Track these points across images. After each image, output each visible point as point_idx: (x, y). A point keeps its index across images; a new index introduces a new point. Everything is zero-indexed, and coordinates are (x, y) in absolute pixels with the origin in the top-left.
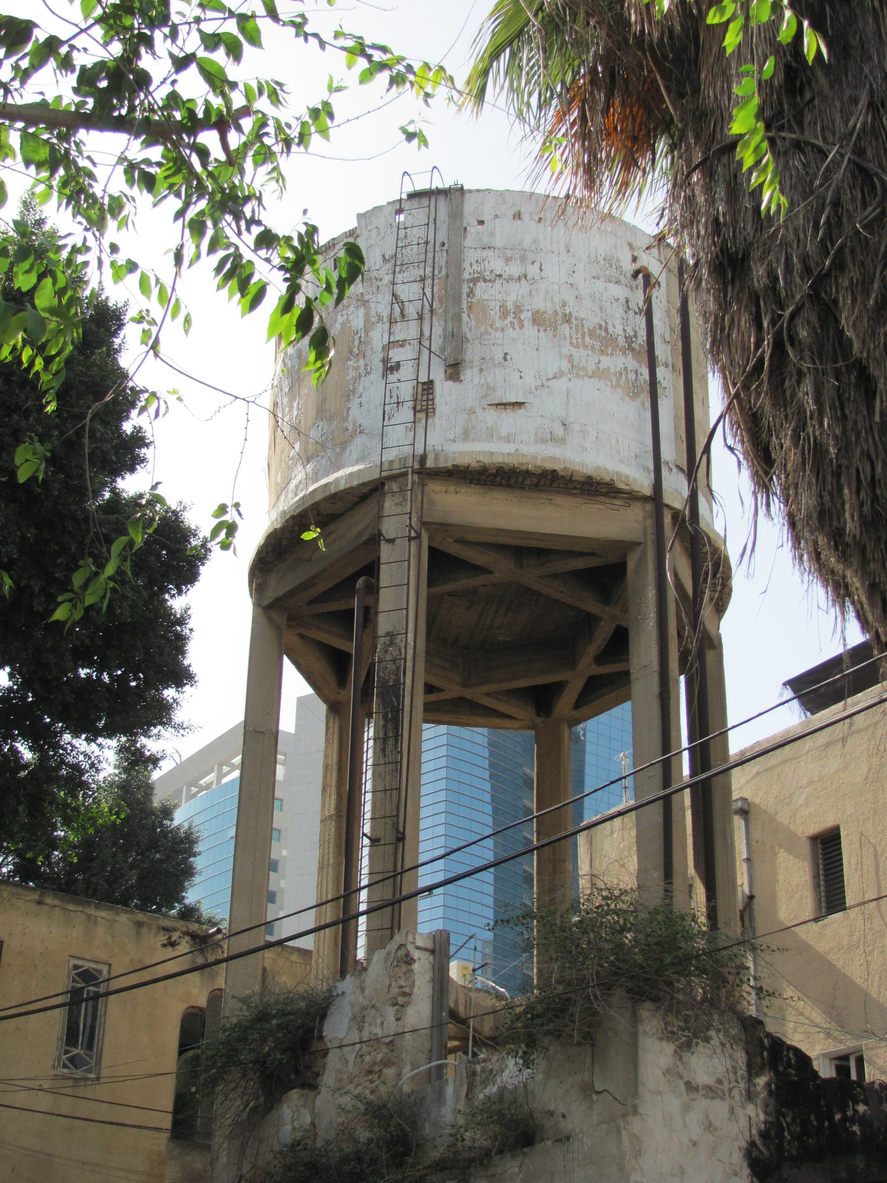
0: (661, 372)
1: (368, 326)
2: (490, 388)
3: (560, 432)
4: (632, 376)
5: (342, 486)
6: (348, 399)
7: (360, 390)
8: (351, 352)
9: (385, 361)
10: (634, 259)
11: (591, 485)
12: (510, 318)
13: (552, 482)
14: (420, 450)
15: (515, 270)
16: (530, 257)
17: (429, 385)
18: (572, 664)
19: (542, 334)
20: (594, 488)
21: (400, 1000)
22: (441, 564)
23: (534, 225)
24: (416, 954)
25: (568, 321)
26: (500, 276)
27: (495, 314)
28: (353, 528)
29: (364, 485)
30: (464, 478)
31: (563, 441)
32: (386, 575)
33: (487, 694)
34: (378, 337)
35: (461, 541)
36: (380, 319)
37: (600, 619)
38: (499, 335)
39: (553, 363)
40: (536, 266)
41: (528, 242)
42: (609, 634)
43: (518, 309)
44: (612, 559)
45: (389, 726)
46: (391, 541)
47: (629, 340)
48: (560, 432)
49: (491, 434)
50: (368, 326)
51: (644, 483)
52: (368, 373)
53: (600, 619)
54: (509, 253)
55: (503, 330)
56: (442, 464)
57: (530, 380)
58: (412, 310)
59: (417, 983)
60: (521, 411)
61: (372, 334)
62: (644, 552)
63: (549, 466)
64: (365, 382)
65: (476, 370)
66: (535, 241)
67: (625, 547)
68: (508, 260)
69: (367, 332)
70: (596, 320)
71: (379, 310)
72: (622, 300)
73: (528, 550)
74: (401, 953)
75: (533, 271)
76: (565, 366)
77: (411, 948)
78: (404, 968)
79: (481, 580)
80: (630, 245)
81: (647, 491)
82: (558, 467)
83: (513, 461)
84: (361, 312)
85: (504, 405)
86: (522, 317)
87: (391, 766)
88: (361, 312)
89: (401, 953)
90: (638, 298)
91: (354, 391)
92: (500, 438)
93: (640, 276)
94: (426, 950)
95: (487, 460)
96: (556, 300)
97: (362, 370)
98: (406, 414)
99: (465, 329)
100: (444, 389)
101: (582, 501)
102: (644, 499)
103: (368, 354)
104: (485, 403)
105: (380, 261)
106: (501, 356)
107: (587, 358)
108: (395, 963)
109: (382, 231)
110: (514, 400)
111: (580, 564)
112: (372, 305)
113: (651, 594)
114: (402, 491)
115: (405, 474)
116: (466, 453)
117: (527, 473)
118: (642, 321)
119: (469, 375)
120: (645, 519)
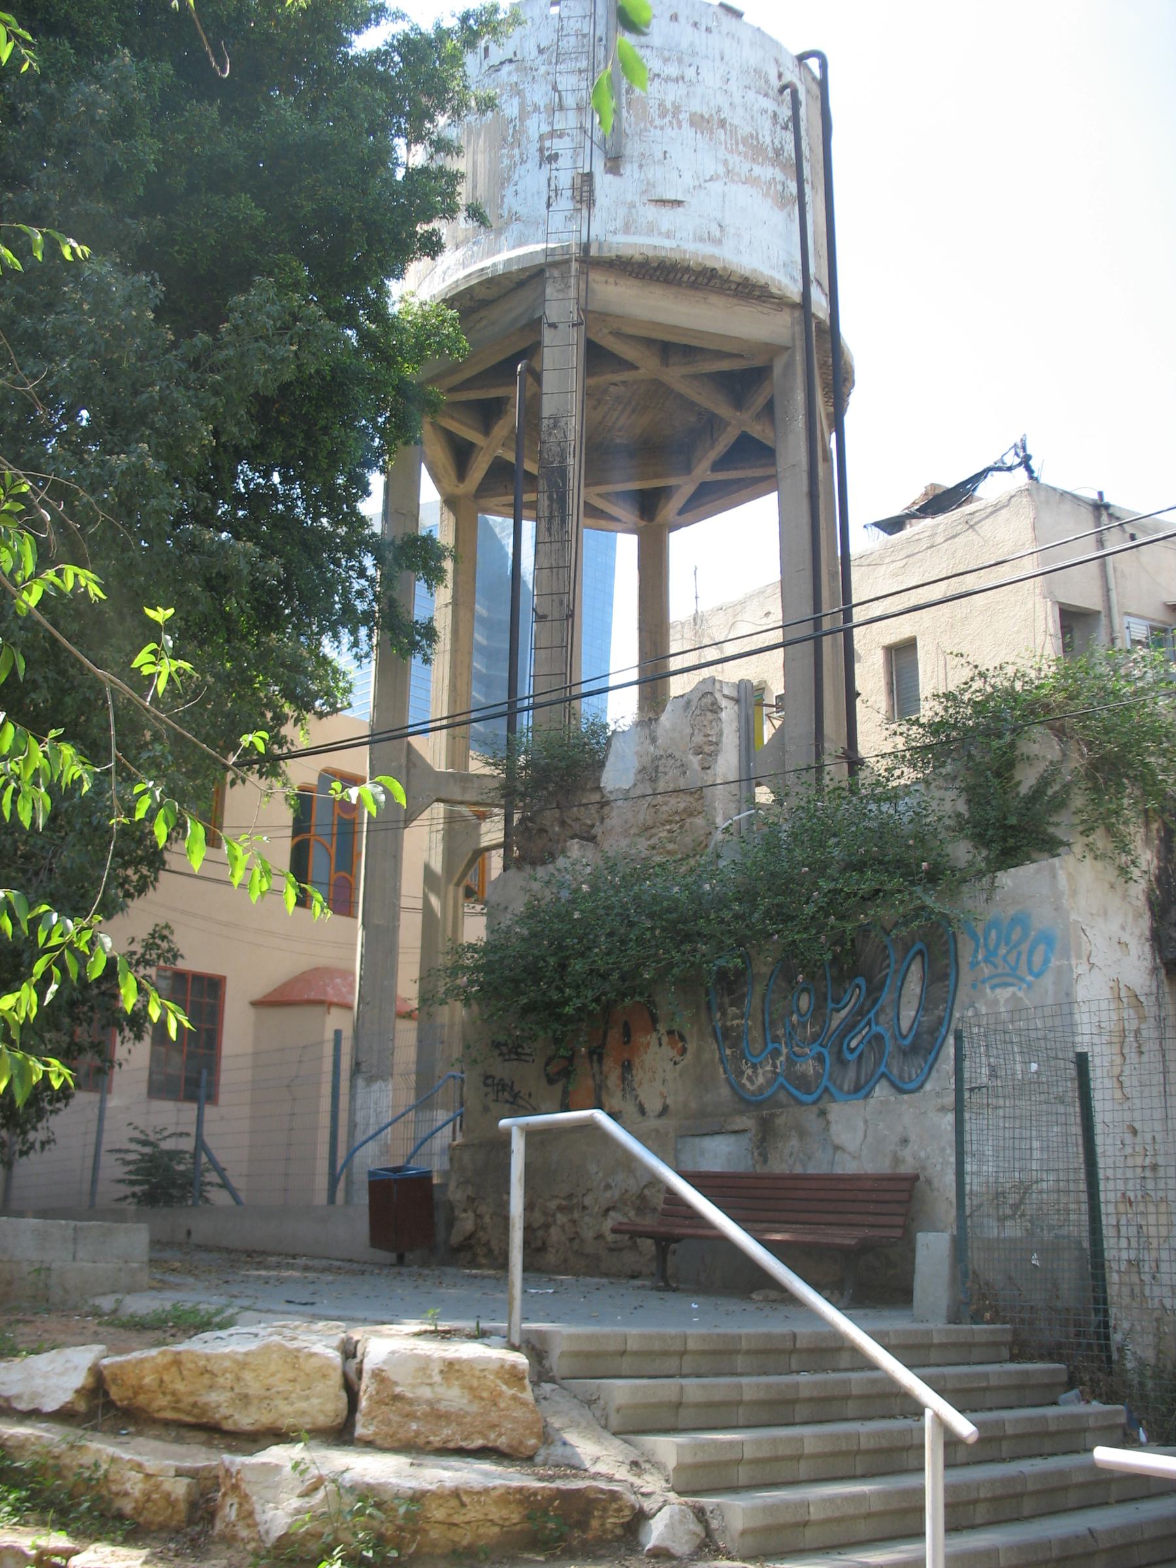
0: (807, 188)
1: (523, 115)
2: (650, 185)
3: (716, 233)
4: (779, 187)
5: (500, 270)
6: (502, 187)
7: (516, 178)
8: (504, 140)
9: (541, 150)
10: (780, 76)
11: (746, 286)
12: (669, 118)
13: (710, 279)
14: (584, 239)
15: (672, 70)
16: (687, 59)
17: (588, 177)
18: (688, 469)
19: (699, 135)
20: (748, 290)
21: (707, 749)
22: (596, 356)
23: (690, 29)
24: (724, 703)
25: (723, 126)
26: (659, 76)
27: (654, 111)
28: (513, 311)
29: (523, 270)
30: (625, 270)
31: (719, 242)
32: (550, 358)
33: (599, 495)
34: (535, 126)
35: (617, 334)
36: (536, 109)
37: (728, 424)
38: (658, 132)
39: (711, 167)
40: (693, 69)
41: (684, 45)
42: (733, 440)
43: (677, 109)
44: (757, 363)
45: (555, 506)
46: (553, 326)
47: (778, 152)
48: (716, 233)
49: (651, 229)
50: (523, 115)
51: (794, 291)
52: (523, 162)
53: (728, 424)
54: (666, 54)
55: (662, 128)
56: (606, 254)
57: (688, 180)
58: (570, 101)
59: (725, 732)
60: (680, 210)
61: (528, 123)
62: (792, 357)
63: (710, 264)
64: (521, 170)
65: (636, 166)
66: (692, 45)
67: (773, 350)
68: (666, 60)
69: (522, 120)
70: (749, 129)
71: (536, 99)
72: (770, 113)
73: (671, 348)
74: (709, 700)
75: (690, 73)
76: (721, 170)
77: (718, 696)
78: (710, 716)
79: (626, 376)
80: (776, 61)
81: (797, 298)
82: (718, 265)
83: (676, 256)
84: (516, 101)
85: (663, 202)
86: (681, 117)
87: (556, 546)
88: (516, 101)
89: (709, 700)
90: (786, 112)
91: (509, 179)
92: (660, 233)
93: (788, 90)
94: (731, 699)
95: (650, 253)
96: (712, 104)
97: (517, 158)
98: (565, 203)
99: (625, 125)
100: (604, 183)
101: (735, 301)
102: (793, 306)
103: (524, 141)
104: (645, 199)
105: (535, 53)
106: (661, 155)
107: (741, 165)
108: (698, 712)
109: (537, 21)
110: (671, 196)
111: (725, 365)
112: (528, 95)
113: (800, 397)
114: (565, 277)
115: (567, 262)
116: (630, 245)
117: (688, 269)
118: (789, 136)
119: (628, 169)
120: (793, 325)
